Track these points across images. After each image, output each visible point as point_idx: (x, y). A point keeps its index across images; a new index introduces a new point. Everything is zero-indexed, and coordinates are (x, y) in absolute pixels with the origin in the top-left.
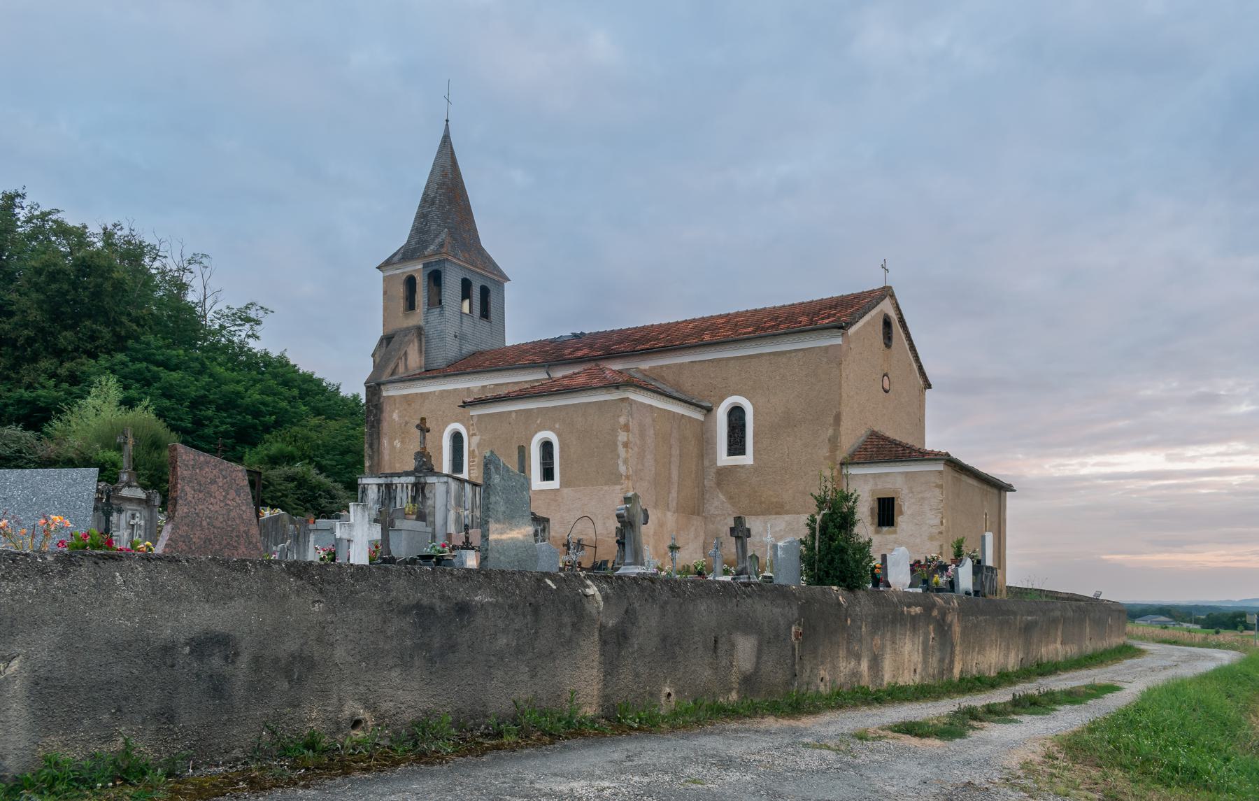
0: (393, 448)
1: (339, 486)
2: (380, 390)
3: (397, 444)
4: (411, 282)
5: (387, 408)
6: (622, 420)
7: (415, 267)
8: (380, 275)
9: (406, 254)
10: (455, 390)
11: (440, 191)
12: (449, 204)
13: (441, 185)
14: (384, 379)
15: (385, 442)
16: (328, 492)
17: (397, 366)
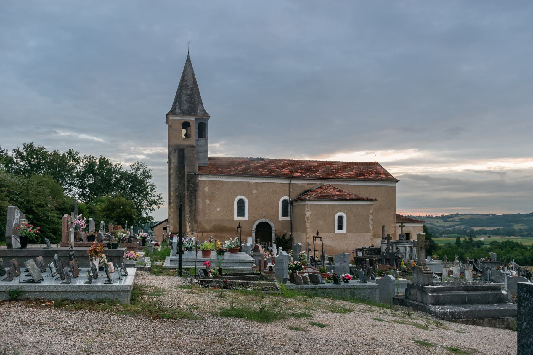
0: (204, 204)
3: (207, 202)
5: (200, 187)
6: (371, 211)
15: (200, 200)
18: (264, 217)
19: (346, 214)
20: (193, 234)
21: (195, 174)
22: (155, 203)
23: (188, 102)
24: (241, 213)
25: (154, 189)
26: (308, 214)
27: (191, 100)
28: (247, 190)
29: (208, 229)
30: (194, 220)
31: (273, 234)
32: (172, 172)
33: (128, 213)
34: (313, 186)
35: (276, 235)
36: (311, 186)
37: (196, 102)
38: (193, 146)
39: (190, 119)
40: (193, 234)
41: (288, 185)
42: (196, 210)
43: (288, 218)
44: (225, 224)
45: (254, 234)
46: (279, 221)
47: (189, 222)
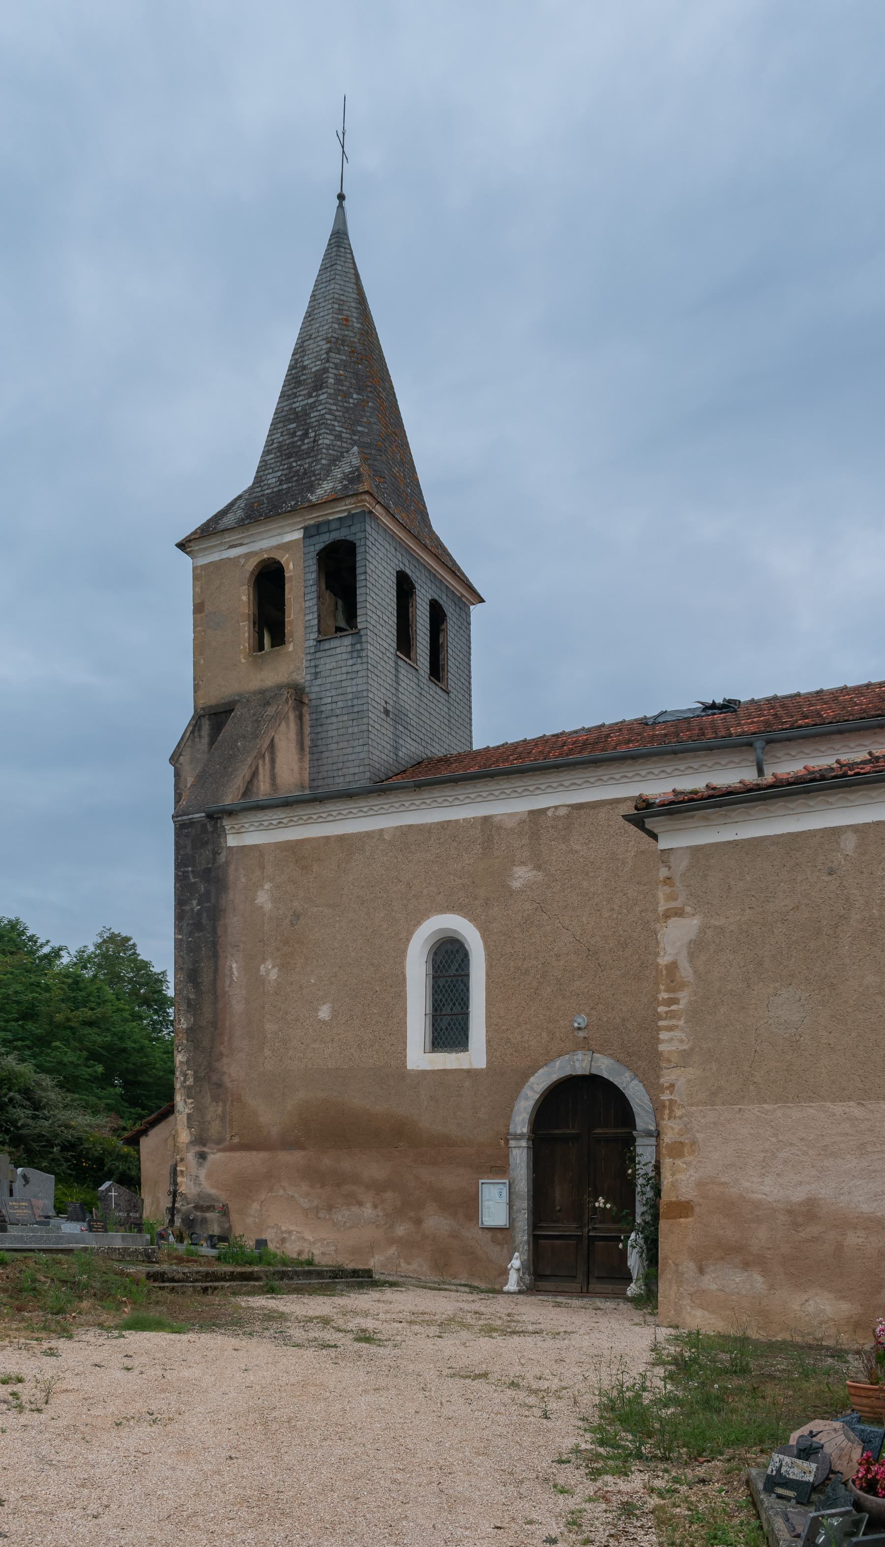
1: (47, 1080)
2: (219, 833)
3: (270, 971)
4: (269, 580)
7: (284, 540)
8: (186, 562)
9: (257, 508)
11: (336, 358)
12: (359, 391)
13: (336, 344)
14: (230, 797)
15: (234, 967)
16: (26, 1092)
17: (255, 774)
18: (586, 1045)
28: (473, 868)
37: (326, 440)
40: (202, 1156)
45: (520, 1157)
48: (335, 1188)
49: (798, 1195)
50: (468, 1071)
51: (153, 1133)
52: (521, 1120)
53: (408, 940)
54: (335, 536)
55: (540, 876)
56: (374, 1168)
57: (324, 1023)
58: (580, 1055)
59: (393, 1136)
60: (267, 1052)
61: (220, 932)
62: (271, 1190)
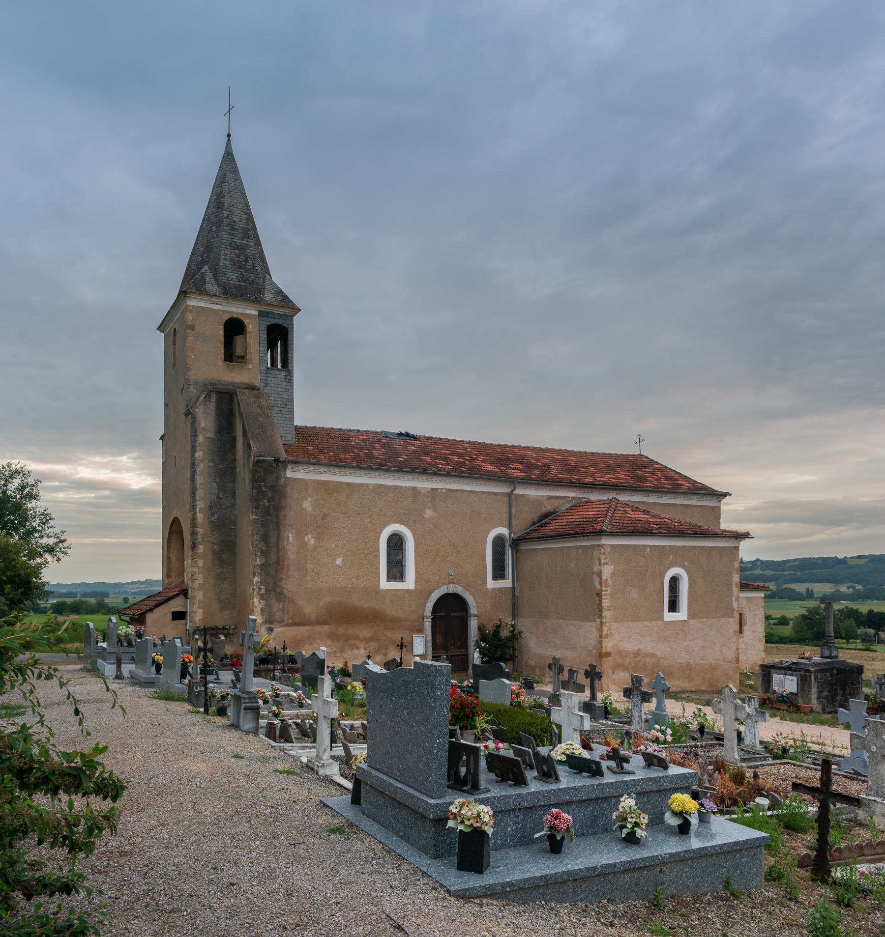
0: (303, 545)
3: (310, 539)
10: (396, 487)
18: (453, 581)
19: (688, 573)
20: (271, 630)
21: (277, 460)
22: (50, 550)
23: (239, 265)
24: (396, 570)
25: (47, 521)
26: (607, 571)
27: (246, 260)
28: (410, 508)
29: (313, 617)
30: (273, 589)
31: (473, 624)
32: (199, 454)
33: (22, 572)
34: (561, 501)
35: (480, 628)
36: (556, 503)
38: (253, 388)
39: (247, 311)
40: (271, 630)
41: (506, 499)
42: (279, 563)
43: (507, 583)
44: (357, 601)
45: (428, 624)
46: (485, 592)
47: (262, 597)
48: (343, 641)
49: (636, 649)
50: (407, 590)
51: (156, 610)
52: (428, 612)
53: (381, 533)
54: (277, 321)
55: (435, 514)
56: (365, 632)
57: (339, 566)
58: (451, 585)
59: (375, 618)
60: (308, 578)
61: (281, 517)
62: (311, 644)
